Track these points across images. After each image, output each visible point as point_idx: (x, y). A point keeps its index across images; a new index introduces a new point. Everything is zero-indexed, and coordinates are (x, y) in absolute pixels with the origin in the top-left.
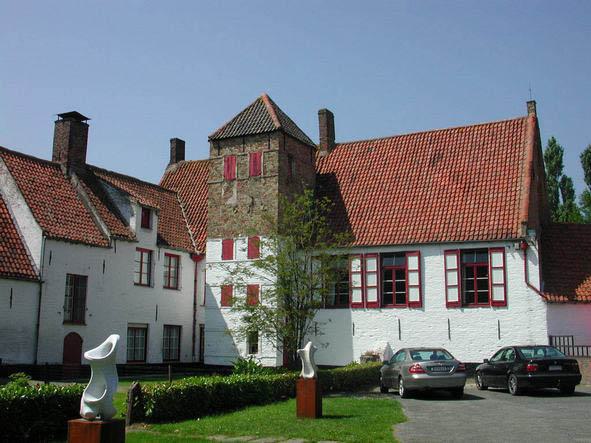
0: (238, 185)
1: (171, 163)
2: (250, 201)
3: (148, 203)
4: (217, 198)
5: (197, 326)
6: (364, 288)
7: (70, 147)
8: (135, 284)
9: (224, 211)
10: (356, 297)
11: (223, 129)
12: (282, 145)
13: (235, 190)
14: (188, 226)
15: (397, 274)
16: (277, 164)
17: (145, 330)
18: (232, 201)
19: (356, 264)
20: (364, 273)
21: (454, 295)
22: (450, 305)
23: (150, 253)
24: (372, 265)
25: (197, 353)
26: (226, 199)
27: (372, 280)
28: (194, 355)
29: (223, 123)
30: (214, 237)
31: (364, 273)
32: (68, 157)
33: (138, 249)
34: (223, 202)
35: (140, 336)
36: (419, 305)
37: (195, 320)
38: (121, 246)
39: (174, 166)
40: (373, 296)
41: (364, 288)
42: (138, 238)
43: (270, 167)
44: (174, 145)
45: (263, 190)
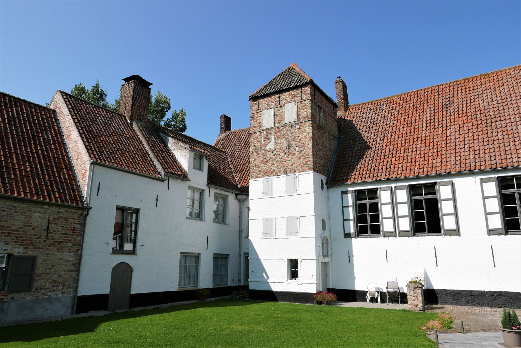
0: (276, 132)
1: (221, 133)
2: (286, 144)
3: (236, 192)
4: (257, 145)
5: (242, 255)
6: (395, 217)
7: (133, 104)
8: (187, 218)
9: (264, 155)
10: (387, 225)
11: (261, 90)
12: (313, 96)
13: (273, 137)
14: (235, 174)
15: (373, 198)
16: (309, 111)
17: (197, 257)
18: (271, 146)
19: (384, 196)
20: (394, 203)
21: (497, 222)
22: (491, 232)
23: (202, 192)
24: (402, 195)
25: (242, 277)
26: (265, 145)
27: (404, 210)
28: (240, 280)
29: (261, 87)
30: (256, 177)
31: (394, 203)
32: (132, 112)
33: (190, 188)
34: (263, 148)
35: (191, 262)
36: (456, 232)
37: (240, 251)
38: (174, 183)
39: (223, 135)
40: (405, 224)
41: (395, 217)
42: (190, 177)
43: (304, 114)
44: (223, 120)
45: (298, 134)
